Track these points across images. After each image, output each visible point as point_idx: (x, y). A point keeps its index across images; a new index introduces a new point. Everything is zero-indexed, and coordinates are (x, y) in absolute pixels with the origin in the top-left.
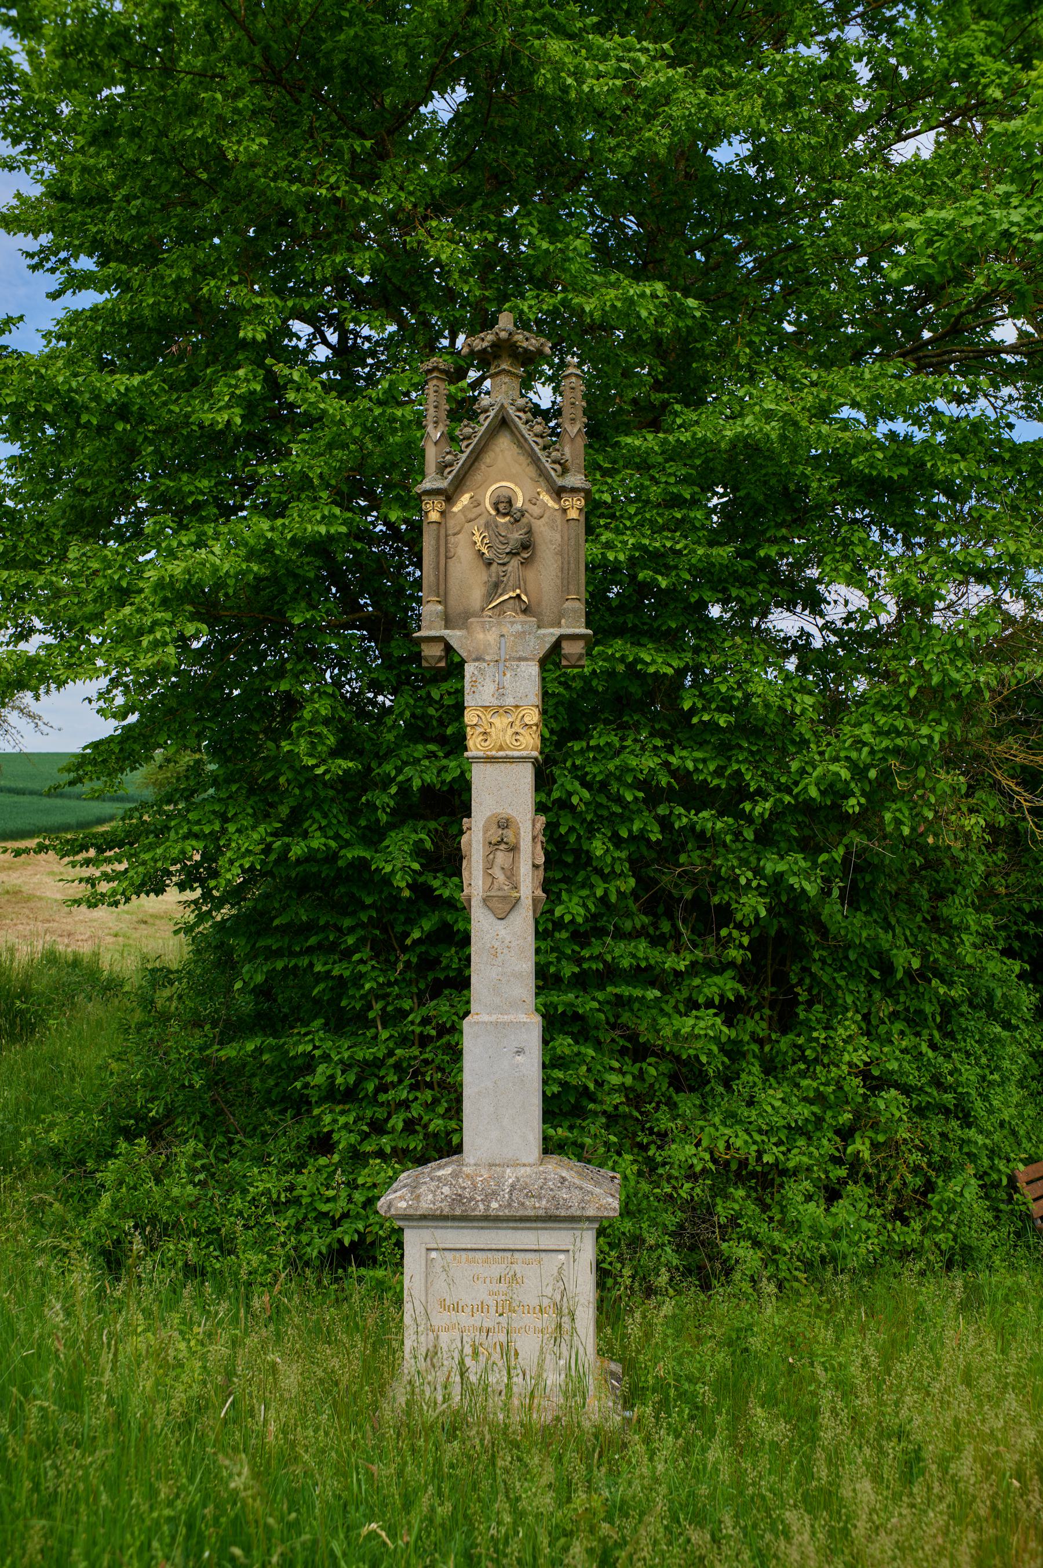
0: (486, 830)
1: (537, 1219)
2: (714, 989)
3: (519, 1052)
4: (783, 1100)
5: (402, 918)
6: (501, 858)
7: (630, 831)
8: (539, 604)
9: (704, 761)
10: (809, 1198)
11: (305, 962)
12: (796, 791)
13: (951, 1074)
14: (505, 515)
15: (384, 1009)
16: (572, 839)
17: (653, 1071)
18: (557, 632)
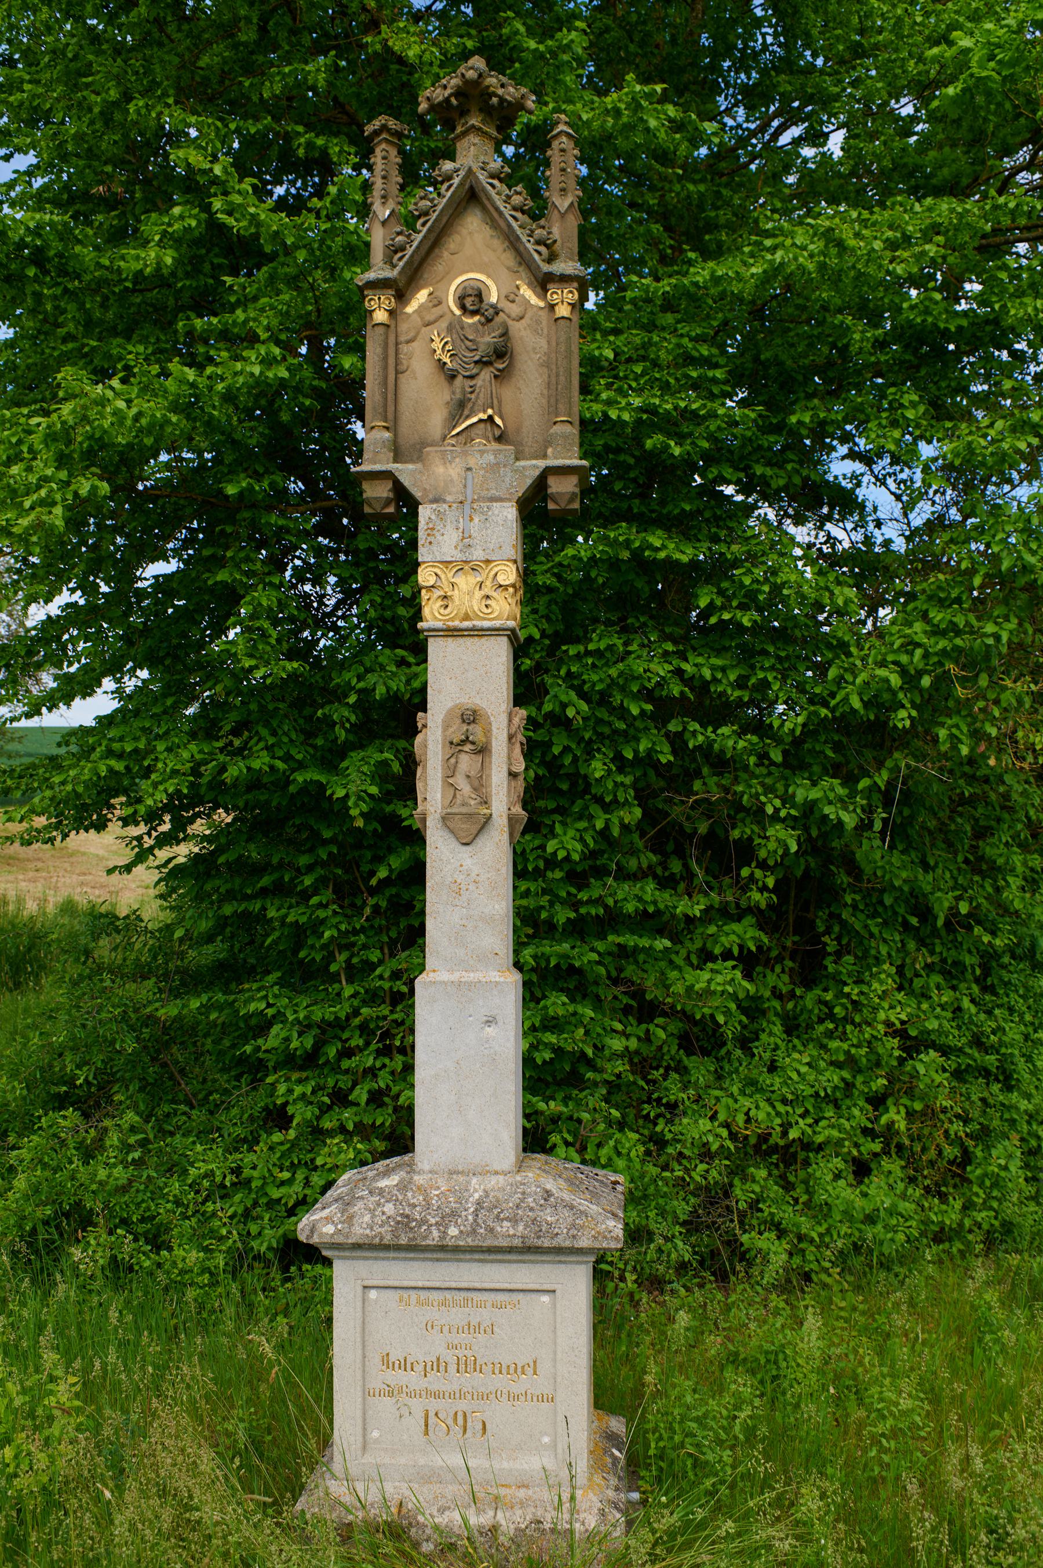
0: (446, 726)
1: (511, 1250)
2: (733, 937)
3: (490, 1022)
4: (808, 1064)
5: (369, 855)
6: (466, 762)
7: (636, 752)
8: (518, 430)
9: (723, 670)
10: (837, 1177)
11: (256, 906)
12: (833, 703)
13: (994, 1033)
14: (474, 313)
15: (348, 961)
16: (567, 760)
17: (662, 1034)
18: (542, 464)
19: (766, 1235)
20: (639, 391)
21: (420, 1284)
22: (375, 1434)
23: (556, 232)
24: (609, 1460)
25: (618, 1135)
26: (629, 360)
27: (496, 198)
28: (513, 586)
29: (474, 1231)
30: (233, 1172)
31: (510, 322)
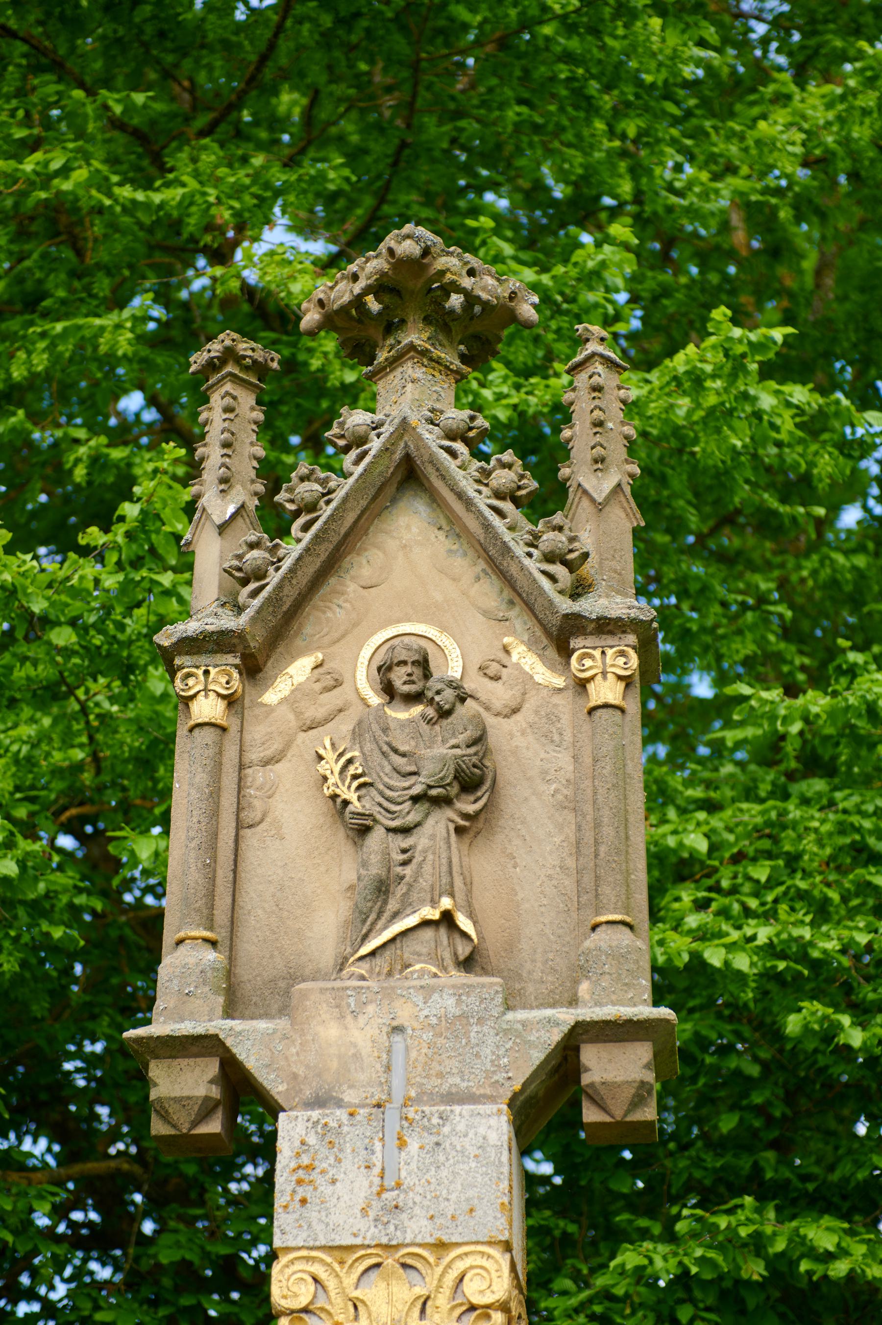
8: (511, 946)
18: (567, 1017)
20: (769, 915)
23: (587, 541)
26: (738, 858)
27: (459, 474)
28: (504, 1307)
31: (490, 720)
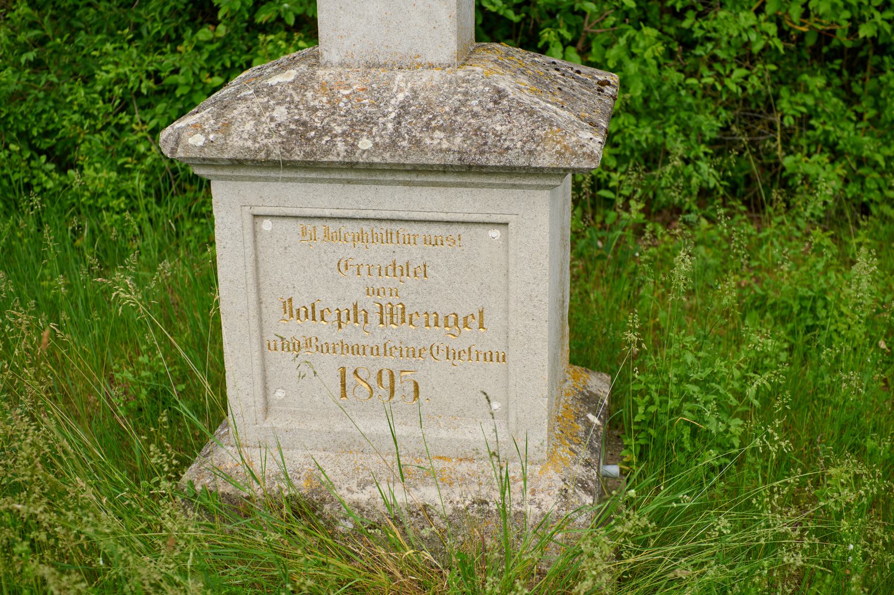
1: (445, 169)
19: (816, 157)
21: (327, 213)
22: (280, 394)
24: (581, 428)
25: (631, 32)
29: (393, 144)
30: (149, 76)
